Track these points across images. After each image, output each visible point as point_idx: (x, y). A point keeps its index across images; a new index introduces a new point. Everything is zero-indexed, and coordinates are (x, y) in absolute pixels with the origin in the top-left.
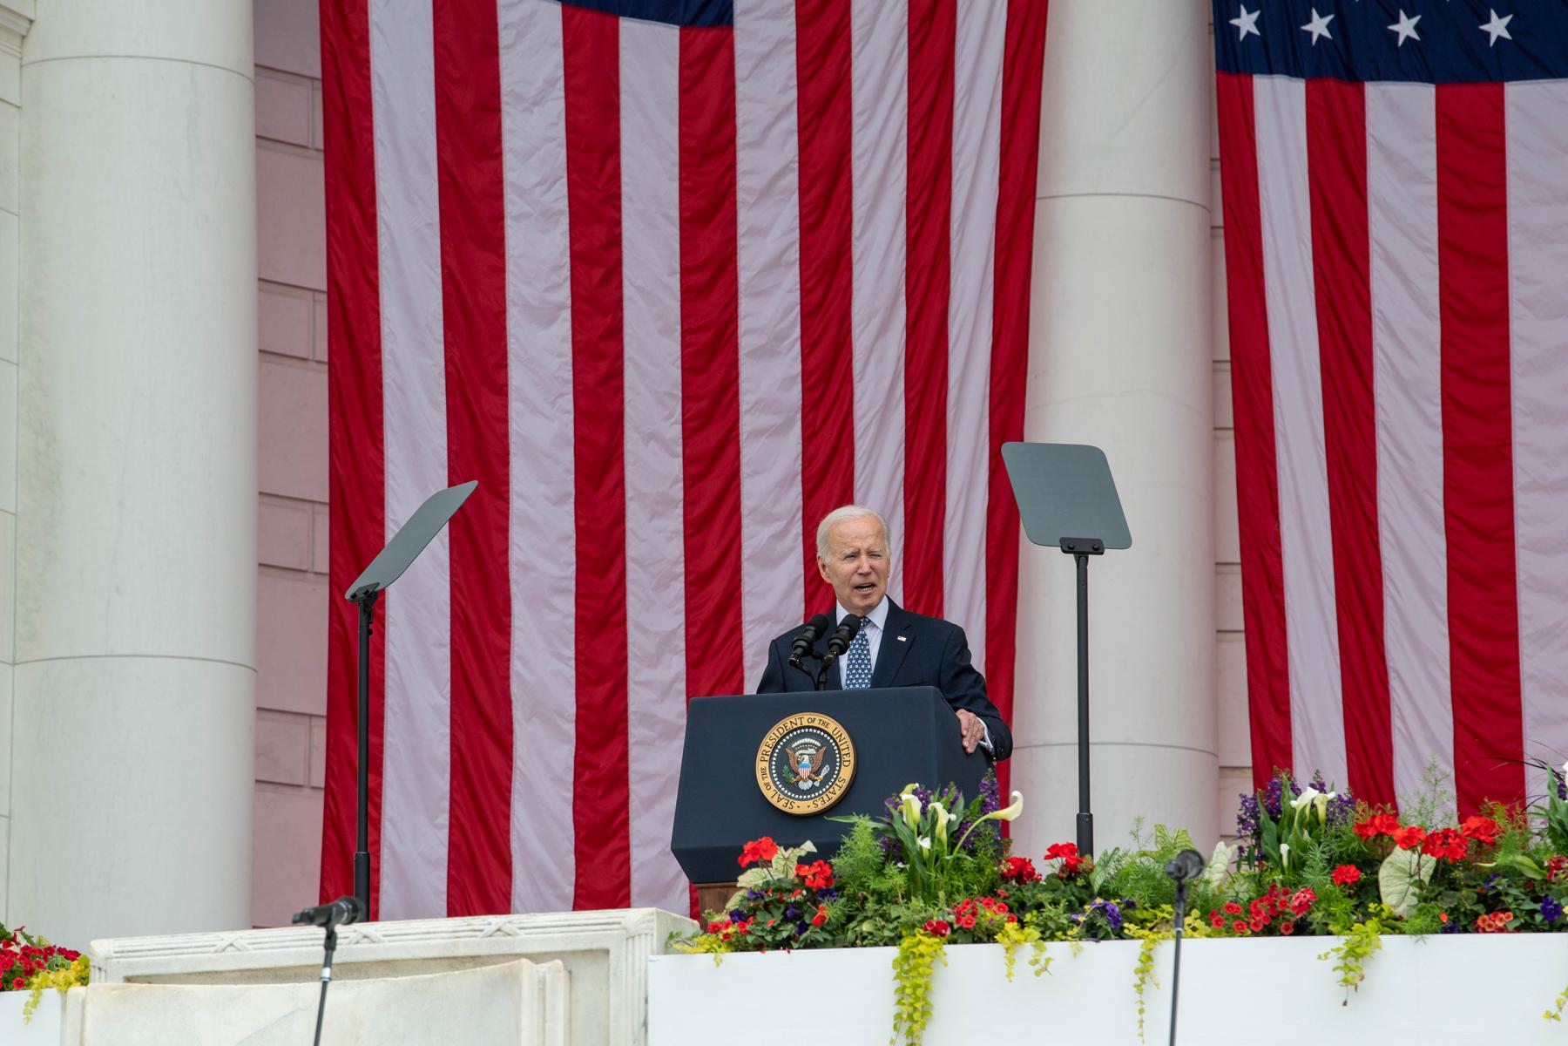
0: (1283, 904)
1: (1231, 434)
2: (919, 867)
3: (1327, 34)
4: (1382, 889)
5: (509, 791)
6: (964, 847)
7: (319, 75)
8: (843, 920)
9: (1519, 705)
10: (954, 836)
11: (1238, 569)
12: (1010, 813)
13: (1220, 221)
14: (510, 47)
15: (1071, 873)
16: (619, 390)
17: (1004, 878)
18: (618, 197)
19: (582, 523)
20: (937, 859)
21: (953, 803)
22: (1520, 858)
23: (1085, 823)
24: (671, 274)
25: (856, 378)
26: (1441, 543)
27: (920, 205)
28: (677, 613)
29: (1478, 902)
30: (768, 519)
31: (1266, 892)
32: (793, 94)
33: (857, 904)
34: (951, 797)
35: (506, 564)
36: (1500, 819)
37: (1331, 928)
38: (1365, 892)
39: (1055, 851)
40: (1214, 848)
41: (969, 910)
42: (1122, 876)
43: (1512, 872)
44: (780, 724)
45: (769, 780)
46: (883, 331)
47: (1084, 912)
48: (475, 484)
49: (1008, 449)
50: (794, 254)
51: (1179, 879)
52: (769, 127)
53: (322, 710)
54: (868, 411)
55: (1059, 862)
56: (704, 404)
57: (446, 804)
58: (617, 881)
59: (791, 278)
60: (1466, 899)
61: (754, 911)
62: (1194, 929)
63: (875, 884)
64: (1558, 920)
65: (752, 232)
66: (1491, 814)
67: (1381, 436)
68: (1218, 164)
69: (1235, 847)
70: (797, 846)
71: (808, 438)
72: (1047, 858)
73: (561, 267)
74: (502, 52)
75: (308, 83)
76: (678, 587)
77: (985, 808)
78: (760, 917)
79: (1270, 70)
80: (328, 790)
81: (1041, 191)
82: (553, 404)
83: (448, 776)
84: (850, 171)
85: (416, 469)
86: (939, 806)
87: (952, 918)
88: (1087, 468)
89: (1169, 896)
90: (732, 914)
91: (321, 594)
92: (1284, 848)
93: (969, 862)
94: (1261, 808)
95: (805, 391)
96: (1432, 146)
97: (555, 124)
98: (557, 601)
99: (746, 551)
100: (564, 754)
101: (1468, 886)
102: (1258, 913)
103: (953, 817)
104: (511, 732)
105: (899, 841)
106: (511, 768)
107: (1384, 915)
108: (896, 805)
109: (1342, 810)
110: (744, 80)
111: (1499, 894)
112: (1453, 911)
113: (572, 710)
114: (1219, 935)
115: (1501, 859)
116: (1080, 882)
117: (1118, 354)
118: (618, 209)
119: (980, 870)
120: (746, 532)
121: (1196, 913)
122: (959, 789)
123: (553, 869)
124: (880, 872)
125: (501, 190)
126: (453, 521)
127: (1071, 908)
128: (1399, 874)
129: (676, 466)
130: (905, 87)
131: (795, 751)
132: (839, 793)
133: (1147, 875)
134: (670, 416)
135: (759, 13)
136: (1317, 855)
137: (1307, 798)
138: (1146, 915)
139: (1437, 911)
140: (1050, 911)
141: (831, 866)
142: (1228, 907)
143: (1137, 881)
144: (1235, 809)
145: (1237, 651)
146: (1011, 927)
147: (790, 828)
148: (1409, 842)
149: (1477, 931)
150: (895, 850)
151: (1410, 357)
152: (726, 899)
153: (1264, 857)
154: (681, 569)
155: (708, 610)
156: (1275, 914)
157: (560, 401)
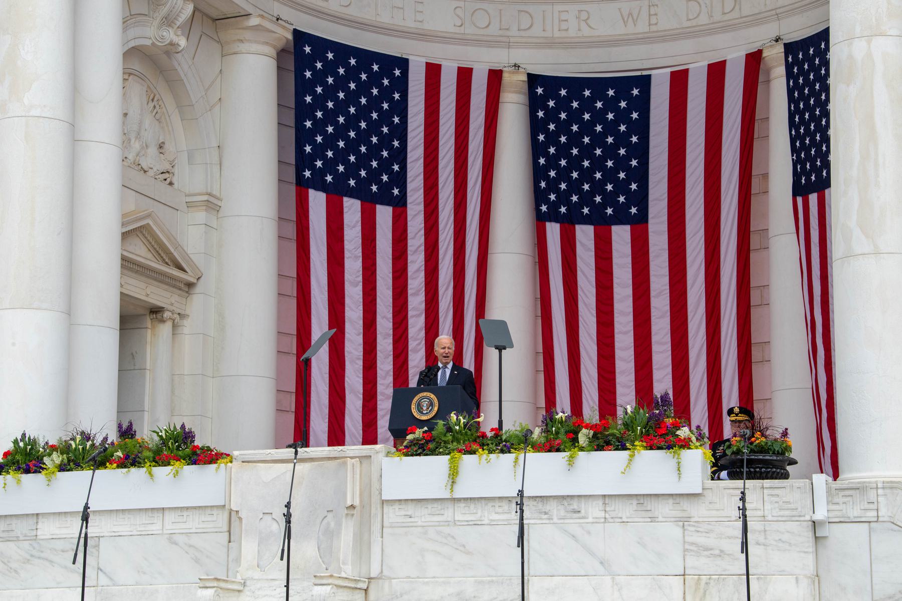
10: (465, 426)
12: (480, 420)
15: (497, 436)
17: (479, 437)
23: (500, 422)
26: (595, 348)
30: (416, 340)
31: (549, 441)
36: (610, 421)
38: (575, 440)
39: (492, 430)
42: (510, 437)
43: (613, 435)
46: (447, 289)
50: (423, 268)
59: (422, 274)
60: (601, 442)
67: (580, 318)
76: (391, 358)
77: (474, 418)
81: (489, 252)
85: (320, 326)
89: (521, 442)
115: (610, 431)
117: (510, 295)
124: (445, 435)
127: (496, 445)
128: (584, 436)
129: (391, 325)
133: (517, 436)
136: (562, 430)
140: (491, 446)
144: (541, 418)
145: (541, 376)
148: (587, 427)
150: (449, 429)
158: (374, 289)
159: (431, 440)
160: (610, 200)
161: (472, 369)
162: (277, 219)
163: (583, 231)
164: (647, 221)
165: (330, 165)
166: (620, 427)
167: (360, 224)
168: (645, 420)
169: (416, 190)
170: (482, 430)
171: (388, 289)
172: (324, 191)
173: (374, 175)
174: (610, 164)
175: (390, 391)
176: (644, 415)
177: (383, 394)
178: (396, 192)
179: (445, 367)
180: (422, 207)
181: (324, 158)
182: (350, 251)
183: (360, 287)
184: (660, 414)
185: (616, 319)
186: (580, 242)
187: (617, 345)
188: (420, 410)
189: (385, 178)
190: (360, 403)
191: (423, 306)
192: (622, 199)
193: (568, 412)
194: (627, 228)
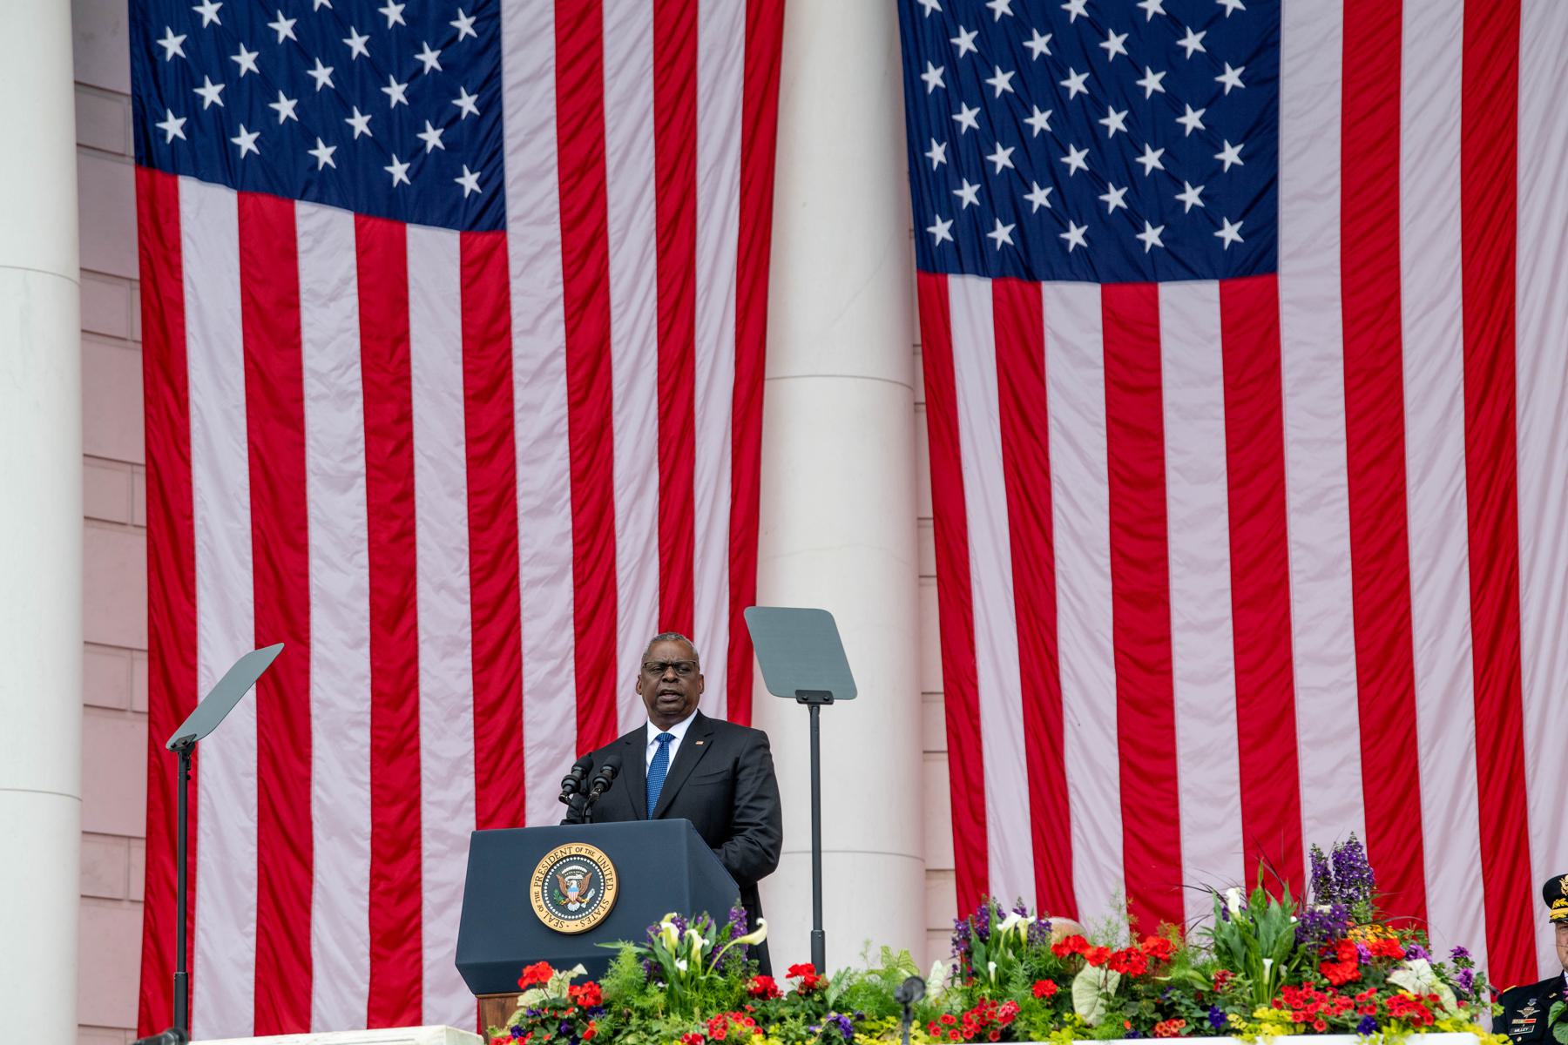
0: (992, 1015)
1: (934, 581)
2: (677, 987)
3: (1009, 240)
4: (1075, 1001)
6: (716, 968)
7: (137, 276)
9: (1177, 815)
10: (707, 959)
11: (942, 697)
13: (922, 398)
14: (309, 251)
15: (809, 989)
16: (412, 546)
23: (818, 941)
24: (457, 445)
26: (1111, 676)
27: (670, 382)
32: (560, 289)
33: (623, 1020)
34: (705, 924)
36: (1174, 939)
38: (1060, 1003)
39: (795, 971)
41: (720, 1024)
42: (852, 992)
43: (1183, 985)
44: (552, 853)
45: (541, 903)
46: (640, 492)
47: (819, 1024)
48: (282, 645)
49: (805, 958)
51: (905, 1003)
52: (540, 317)
53: (141, 831)
55: (798, 980)
57: (254, 915)
60: (1145, 1008)
63: (638, 1002)
64: (1223, 1026)
67: (1060, 583)
68: (919, 349)
69: (950, 965)
74: (300, 256)
75: (127, 283)
76: (469, 717)
77: (734, 934)
78: (538, 1032)
80: (147, 903)
81: (767, 375)
82: (350, 560)
83: (255, 890)
85: (226, 638)
86: (693, 933)
87: (705, 1031)
88: (817, 628)
90: (513, 1030)
91: (139, 731)
92: (992, 966)
93: (720, 981)
94: (972, 930)
97: (349, 317)
98: (353, 733)
100: (360, 868)
102: (970, 1023)
103: (707, 942)
105: (659, 963)
107: (1077, 1023)
111: (1174, 1004)
112: (1136, 1019)
113: (368, 828)
115: (1176, 973)
116: (817, 997)
117: (837, 525)
118: (409, 388)
119: (730, 988)
123: (349, 969)
124: (642, 991)
126: (260, 683)
127: (808, 1021)
128: (1089, 990)
129: (464, 612)
130: (653, 181)
132: (603, 913)
133: (874, 991)
136: (1020, 971)
138: (873, 1026)
139: (1121, 1020)
140: (790, 1024)
142: (945, 1018)
145: (941, 770)
146: (757, 1039)
148: (1098, 958)
149: (1155, 1036)
150: (656, 972)
151: (1083, 515)
152: (505, 1013)
153: (976, 974)
154: (470, 701)
155: (493, 739)
156: (984, 1024)
159: (598, 1007)
162: (75, 274)
164: (1272, 269)
165: (247, 101)
166: (1207, 957)
167: (353, 288)
168: (1287, 936)
169: (533, 175)
171: (452, 495)
172: (230, 182)
173: (395, 132)
175: (467, 823)
176: (1285, 919)
177: (439, 835)
178: (469, 182)
180: (554, 231)
181: (226, 73)
184: (1336, 917)
185: (1175, 584)
186: (1057, 337)
187: (1180, 666)
188: (558, 903)
189: (432, 137)
191: (567, 549)
192: (1191, 197)
194: (1210, 290)
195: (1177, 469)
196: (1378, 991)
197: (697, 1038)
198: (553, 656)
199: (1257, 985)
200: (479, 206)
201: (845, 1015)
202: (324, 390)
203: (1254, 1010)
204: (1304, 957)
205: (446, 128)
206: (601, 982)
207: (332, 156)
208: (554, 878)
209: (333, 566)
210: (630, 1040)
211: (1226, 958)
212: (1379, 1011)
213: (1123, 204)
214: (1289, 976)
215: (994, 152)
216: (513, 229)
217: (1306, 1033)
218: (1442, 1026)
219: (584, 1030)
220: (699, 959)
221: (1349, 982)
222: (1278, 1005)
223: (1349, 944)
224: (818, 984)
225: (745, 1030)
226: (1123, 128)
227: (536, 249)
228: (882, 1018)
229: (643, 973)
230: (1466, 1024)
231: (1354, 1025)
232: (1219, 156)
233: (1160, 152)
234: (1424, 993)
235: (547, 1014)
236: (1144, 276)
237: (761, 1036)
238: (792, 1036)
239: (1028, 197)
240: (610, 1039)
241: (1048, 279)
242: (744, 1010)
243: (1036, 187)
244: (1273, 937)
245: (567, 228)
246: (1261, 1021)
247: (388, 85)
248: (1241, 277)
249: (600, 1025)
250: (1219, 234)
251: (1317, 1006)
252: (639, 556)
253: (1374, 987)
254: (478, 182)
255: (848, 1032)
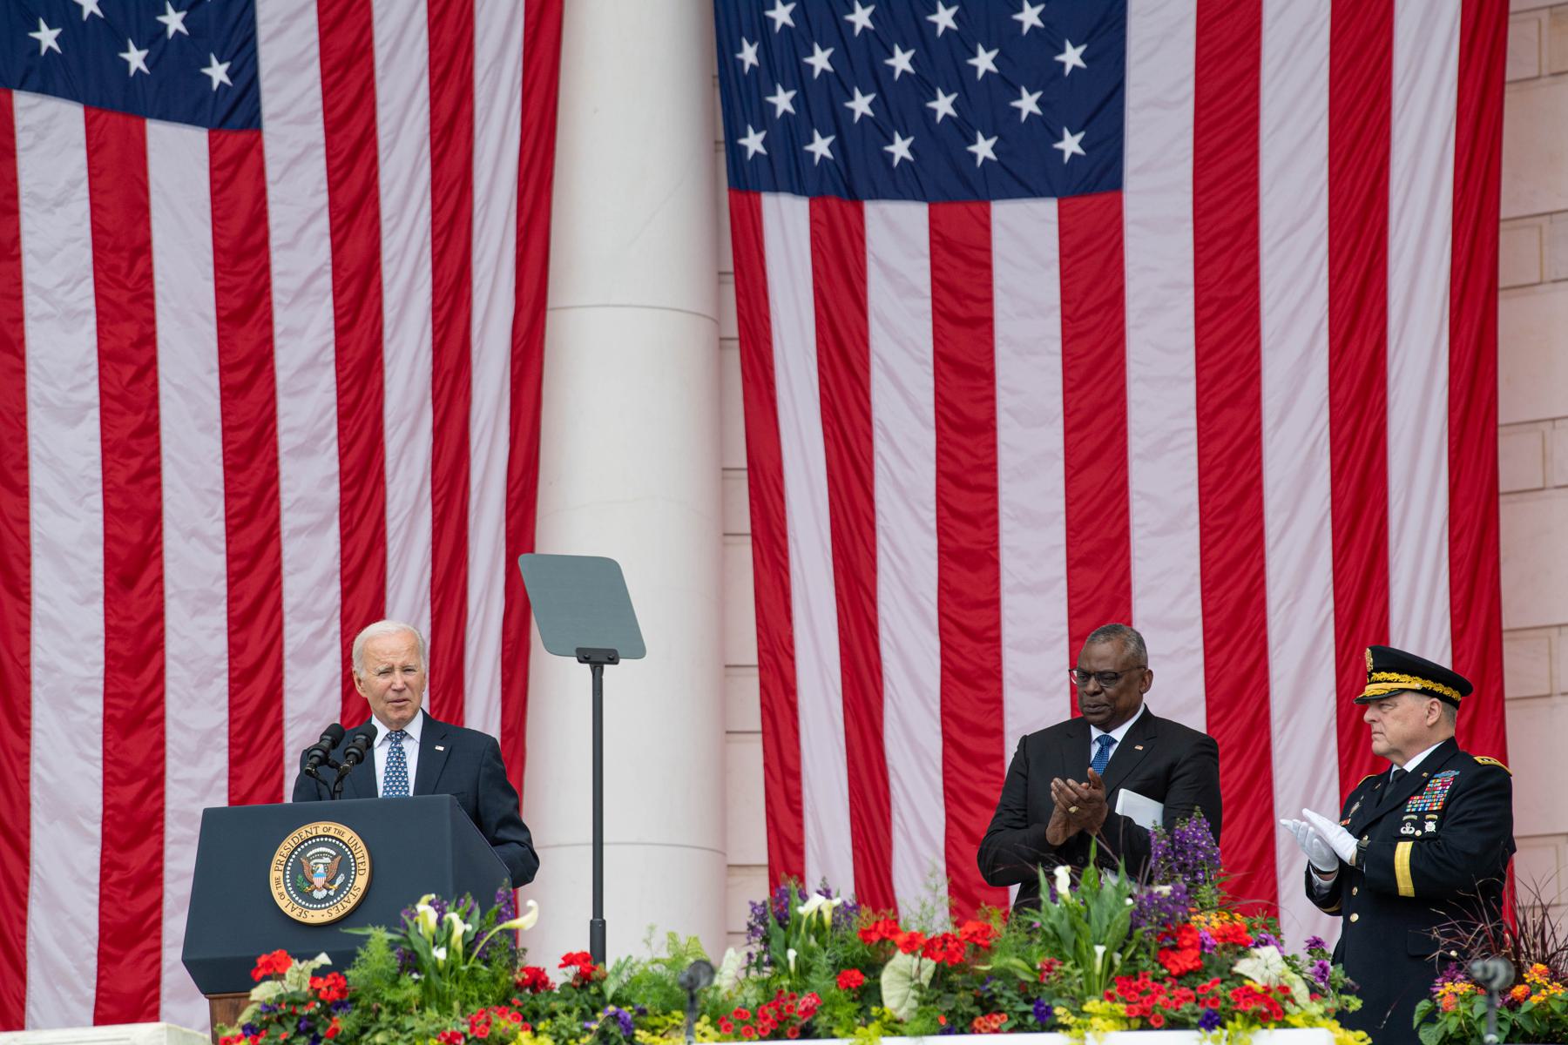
0: (790, 1009)
2: (434, 978)
3: (828, 154)
5: (26, 895)
6: (479, 957)
8: (357, 1031)
10: (469, 946)
12: (522, 923)
15: (586, 980)
16: (157, 487)
17: (519, 987)
18: (151, 296)
19: (112, 622)
20: (452, 969)
21: (469, 914)
22: (1014, 961)
23: (598, 930)
24: (210, 372)
25: (388, 478)
28: (220, 710)
29: (975, 1004)
31: (773, 997)
32: (324, 198)
33: (371, 1016)
34: (467, 907)
35: (28, 666)
37: (835, 1032)
38: (867, 995)
39: (569, 960)
40: (723, 954)
41: (483, 1020)
42: (634, 983)
43: (1006, 975)
44: (295, 833)
45: (283, 889)
46: (412, 433)
47: (596, 1020)
50: (330, 355)
51: (690, 989)
54: (400, 511)
55: (573, 970)
56: (247, 500)
58: (144, 983)
59: (327, 379)
60: (963, 1001)
61: (267, 1024)
62: (704, 1035)
63: (389, 995)
65: (287, 332)
66: (988, 917)
67: (882, 540)
69: (744, 953)
70: (311, 957)
71: (345, 538)
72: (561, 966)
73: (87, 366)
76: (222, 684)
77: (500, 918)
78: (273, 1030)
79: (775, 189)
81: (550, 303)
82: (80, 503)
84: (380, 276)
86: (454, 917)
87: (466, 1028)
90: (244, 1028)
92: (792, 954)
95: (344, 490)
96: (926, 263)
97: (79, 225)
99: (288, 649)
101: (966, 989)
102: (765, 1018)
103: (469, 927)
104: (27, 835)
105: (415, 952)
106: (27, 872)
107: (886, 1018)
108: (412, 917)
109: (847, 917)
110: (274, 183)
111: (993, 997)
112: (951, 1013)
113: (98, 810)
114: (728, 1040)
115: (997, 962)
116: (593, 990)
117: (630, 455)
118: (152, 307)
119: (495, 980)
120: (288, 629)
121: (705, 1019)
122: (475, 899)
124: (395, 983)
125: (21, 290)
127: (583, 1016)
128: (901, 977)
129: (219, 563)
131: (309, 860)
132: (354, 901)
133: (659, 982)
134: (212, 513)
135: (283, 119)
136: (823, 960)
137: (813, 905)
138: (657, 1021)
139: (936, 1014)
140: (563, 1019)
141: (345, 978)
142: (736, 1013)
143: (649, 988)
144: (742, 918)
146: (524, 1036)
147: (304, 939)
148: (910, 945)
149: (973, 1032)
150: (411, 961)
152: (237, 1011)
154: (224, 665)
155: (250, 708)
156: (782, 1019)
157: (88, 500)
158: (150, 429)
159: (343, 1000)
160: (985, 105)
161: (495, 731)
163: (891, 225)
164: (1117, 186)
168: (1122, 921)
170: (531, 960)
174: (901, 61)
178: (218, 72)
179: (398, 734)
182: (44, 293)
183: (91, 426)
184: (1173, 899)
186: (880, 263)
188: (303, 893)
190: (90, 856)
191: (333, 494)
192: (1028, 104)
193: (846, 891)
194: (1045, 211)
195: (1007, 410)
196: (1222, 982)
197: (456, 1036)
198: (317, 616)
199: (1088, 975)
200: (231, 99)
201: (626, 1009)
202: (49, 309)
203: (1084, 1003)
204: (1141, 944)
205: (189, 10)
206: (348, 973)
207: (57, 39)
208: (298, 861)
209: (59, 510)
210: (380, 1038)
211: (1054, 945)
212: (1222, 1004)
213: (952, 112)
214: (1123, 966)
215: (812, 53)
216: (269, 128)
217: (1142, 1028)
218: (1293, 1021)
219: (326, 1027)
220: (460, 947)
221: (1189, 972)
222: (1110, 997)
223: (1191, 930)
224: (595, 975)
225: (511, 1027)
226: (953, 25)
227: (298, 151)
228: (666, 1013)
229: (396, 963)
230: (1319, 1019)
231: (1195, 1020)
232: (1060, 58)
233: (993, 53)
234: (1274, 985)
235: (284, 1009)
236: (976, 194)
237: (529, 1033)
238: (565, 1033)
239: (850, 105)
240: (357, 1038)
241: (871, 198)
242: (510, 1004)
243: (857, 93)
244: (1106, 921)
245: (332, 128)
246: (1090, 1015)
247: (209, 65)
248: (1082, 194)
249: (344, 1022)
250: (1059, 146)
251: (1153, 999)
252: (410, 506)
253: (1217, 978)
254: (228, 73)
255: (629, 1029)
